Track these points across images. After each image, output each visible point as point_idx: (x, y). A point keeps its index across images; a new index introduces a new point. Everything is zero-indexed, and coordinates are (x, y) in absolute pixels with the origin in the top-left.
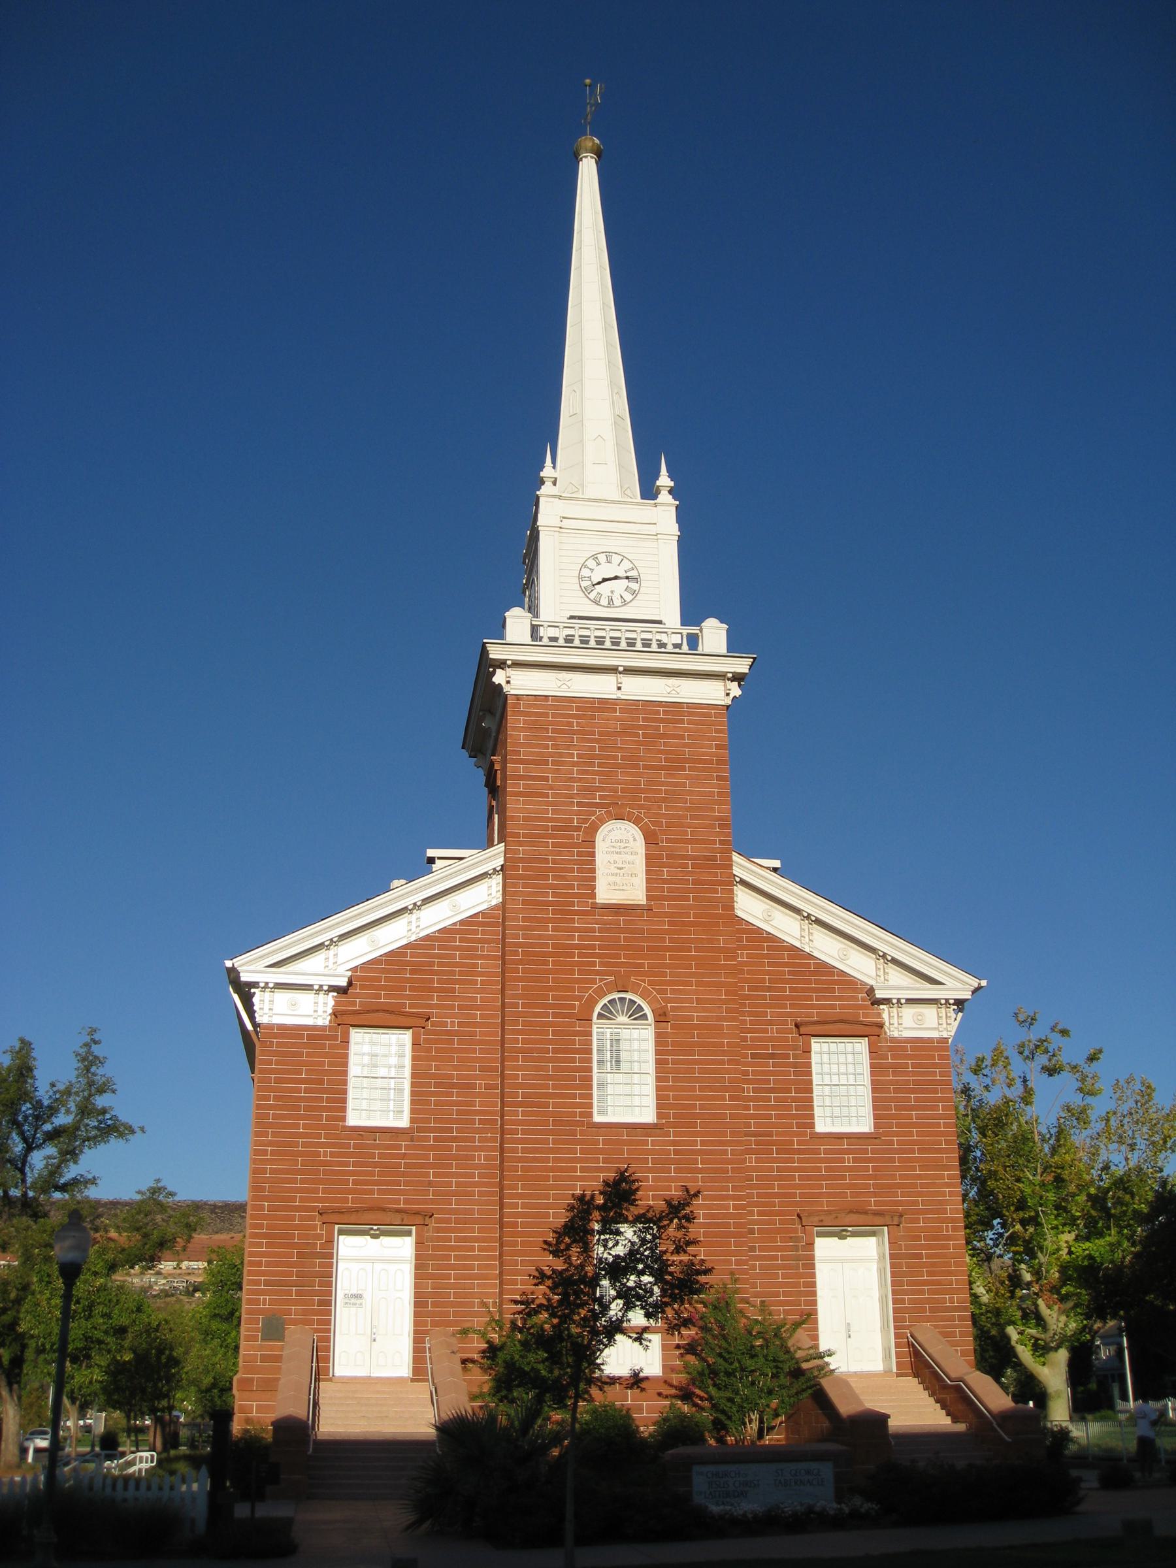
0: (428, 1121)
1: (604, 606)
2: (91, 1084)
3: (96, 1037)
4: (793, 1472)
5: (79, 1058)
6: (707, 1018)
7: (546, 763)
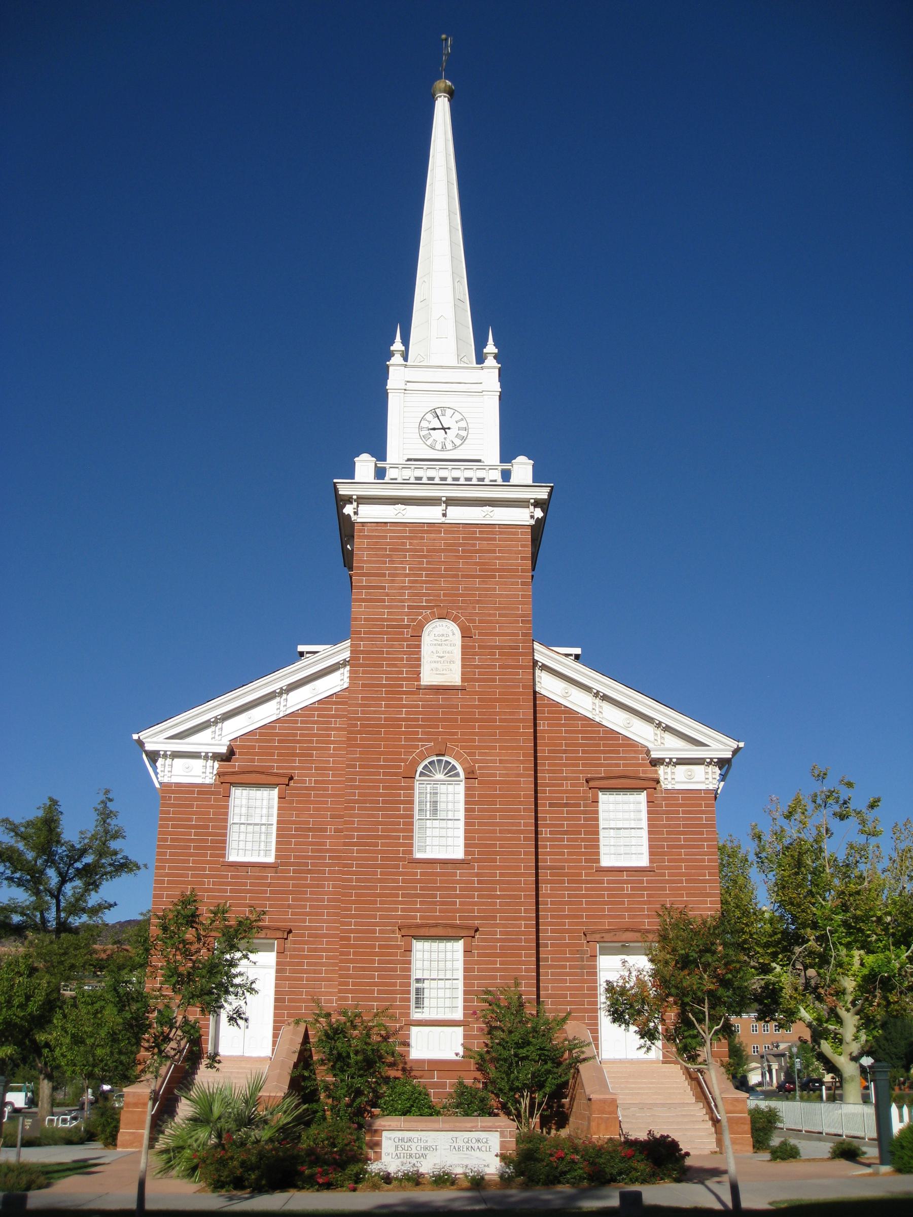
0: (289, 857)
1: (438, 450)
2: (106, 832)
3: (110, 796)
4: (466, 1140)
5: (97, 812)
6: (507, 775)
7: (384, 575)
